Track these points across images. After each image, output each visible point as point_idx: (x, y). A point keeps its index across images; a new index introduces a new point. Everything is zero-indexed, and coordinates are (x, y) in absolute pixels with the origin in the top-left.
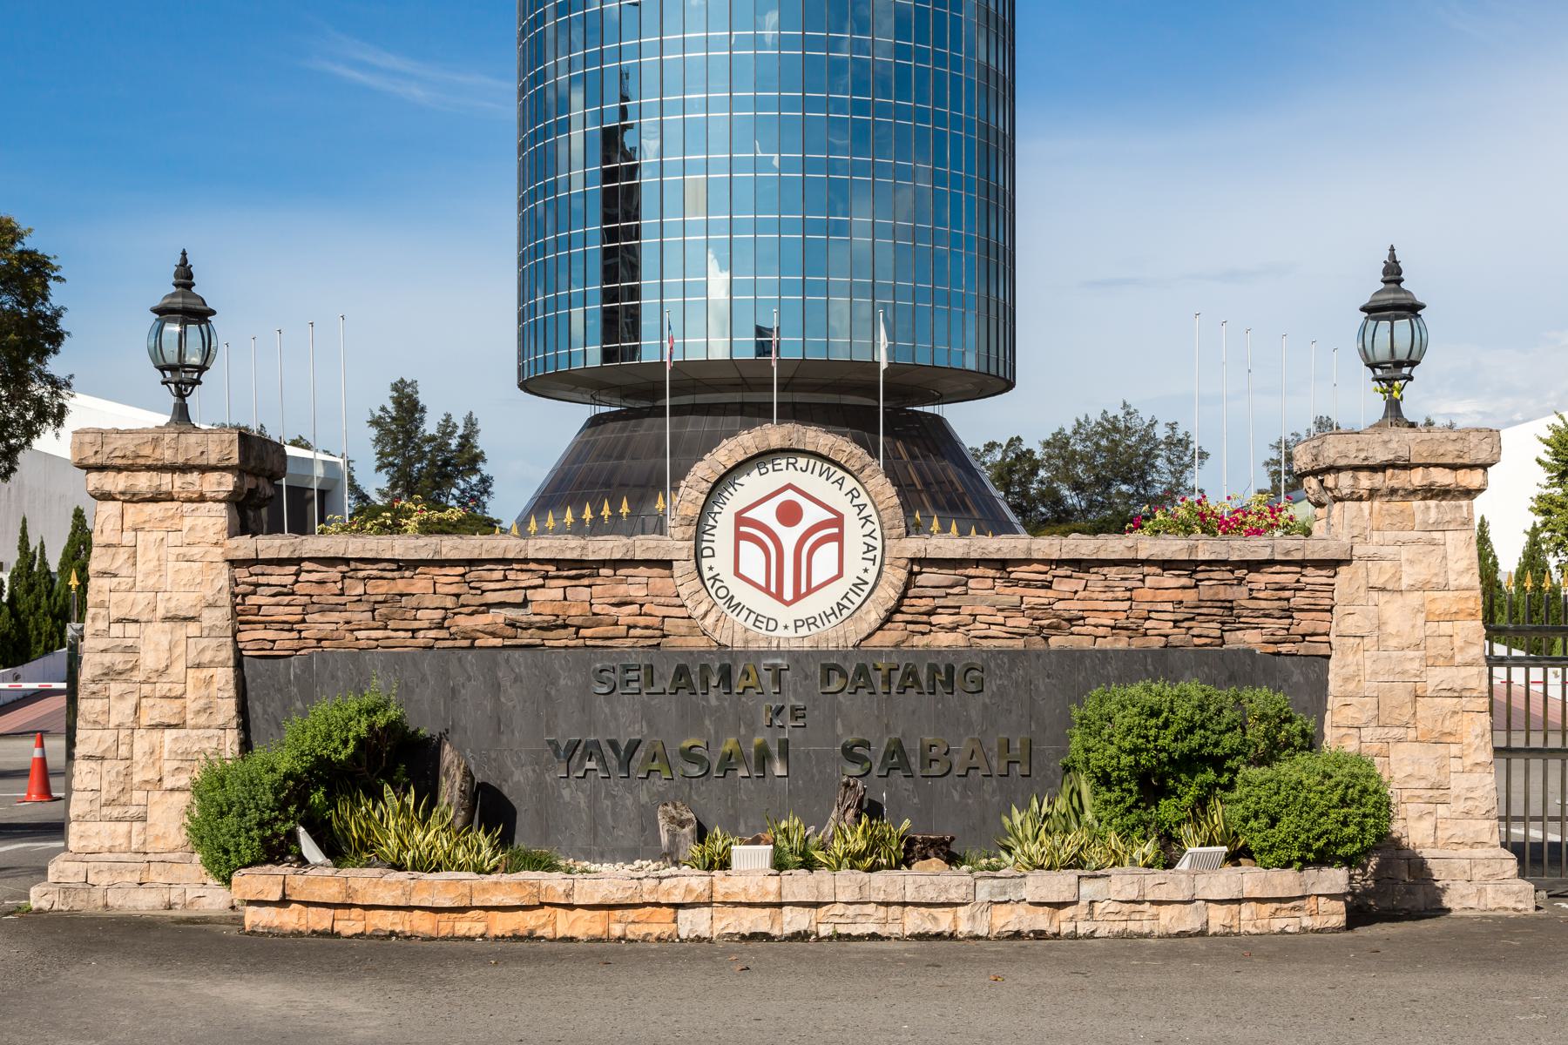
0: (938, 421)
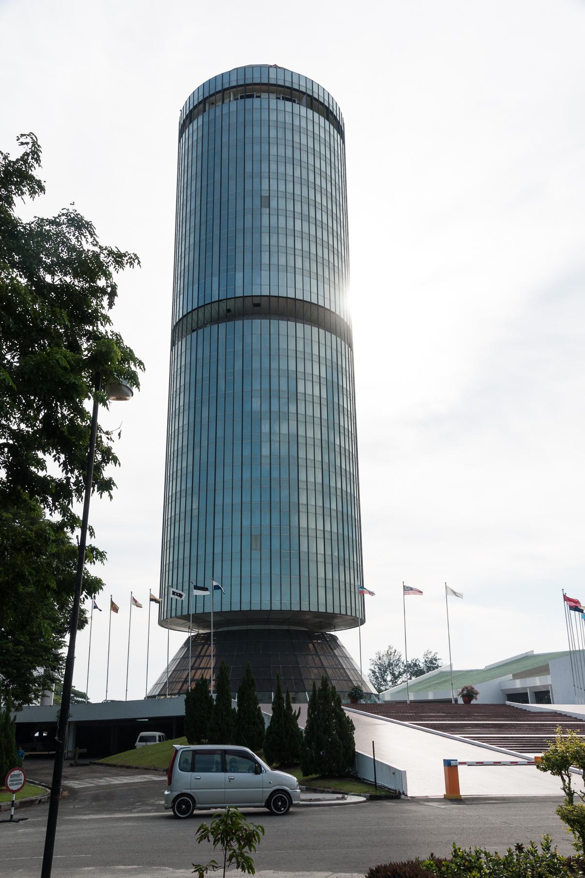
0: (334, 639)
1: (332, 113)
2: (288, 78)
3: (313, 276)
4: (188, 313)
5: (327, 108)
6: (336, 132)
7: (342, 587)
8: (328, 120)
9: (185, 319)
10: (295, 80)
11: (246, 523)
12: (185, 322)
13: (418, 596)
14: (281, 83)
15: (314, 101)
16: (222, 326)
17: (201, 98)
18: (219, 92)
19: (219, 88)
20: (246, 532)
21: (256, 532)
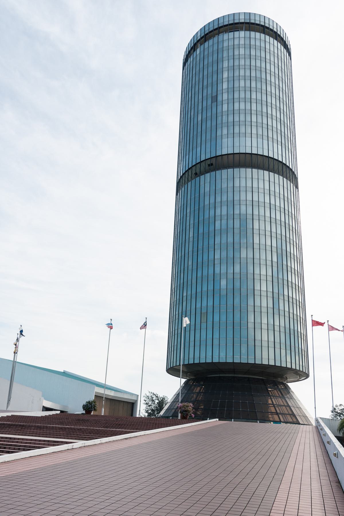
1: (279, 36)
2: (262, 20)
3: (265, 138)
4: (189, 169)
5: (276, 33)
6: (282, 47)
7: (295, 318)
8: (276, 39)
9: (187, 173)
10: (267, 22)
11: (198, 306)
12: (187, 176)
13: (320, 327)
14: (258, 22)
15: (266, 29)
16: (208, 175)
17: (203, 35)
18: (216, 29)
19: (216, 27)
20: (198, 311)
21: (204, 311)
